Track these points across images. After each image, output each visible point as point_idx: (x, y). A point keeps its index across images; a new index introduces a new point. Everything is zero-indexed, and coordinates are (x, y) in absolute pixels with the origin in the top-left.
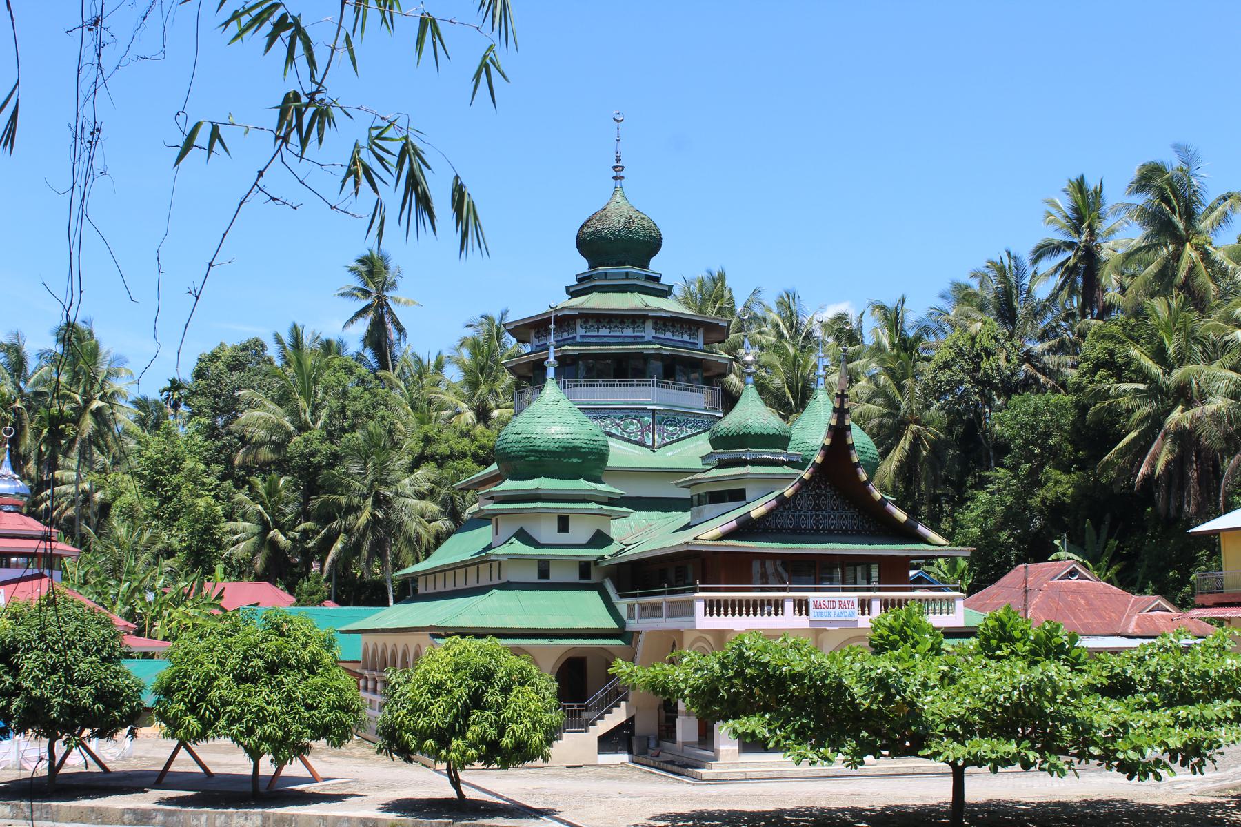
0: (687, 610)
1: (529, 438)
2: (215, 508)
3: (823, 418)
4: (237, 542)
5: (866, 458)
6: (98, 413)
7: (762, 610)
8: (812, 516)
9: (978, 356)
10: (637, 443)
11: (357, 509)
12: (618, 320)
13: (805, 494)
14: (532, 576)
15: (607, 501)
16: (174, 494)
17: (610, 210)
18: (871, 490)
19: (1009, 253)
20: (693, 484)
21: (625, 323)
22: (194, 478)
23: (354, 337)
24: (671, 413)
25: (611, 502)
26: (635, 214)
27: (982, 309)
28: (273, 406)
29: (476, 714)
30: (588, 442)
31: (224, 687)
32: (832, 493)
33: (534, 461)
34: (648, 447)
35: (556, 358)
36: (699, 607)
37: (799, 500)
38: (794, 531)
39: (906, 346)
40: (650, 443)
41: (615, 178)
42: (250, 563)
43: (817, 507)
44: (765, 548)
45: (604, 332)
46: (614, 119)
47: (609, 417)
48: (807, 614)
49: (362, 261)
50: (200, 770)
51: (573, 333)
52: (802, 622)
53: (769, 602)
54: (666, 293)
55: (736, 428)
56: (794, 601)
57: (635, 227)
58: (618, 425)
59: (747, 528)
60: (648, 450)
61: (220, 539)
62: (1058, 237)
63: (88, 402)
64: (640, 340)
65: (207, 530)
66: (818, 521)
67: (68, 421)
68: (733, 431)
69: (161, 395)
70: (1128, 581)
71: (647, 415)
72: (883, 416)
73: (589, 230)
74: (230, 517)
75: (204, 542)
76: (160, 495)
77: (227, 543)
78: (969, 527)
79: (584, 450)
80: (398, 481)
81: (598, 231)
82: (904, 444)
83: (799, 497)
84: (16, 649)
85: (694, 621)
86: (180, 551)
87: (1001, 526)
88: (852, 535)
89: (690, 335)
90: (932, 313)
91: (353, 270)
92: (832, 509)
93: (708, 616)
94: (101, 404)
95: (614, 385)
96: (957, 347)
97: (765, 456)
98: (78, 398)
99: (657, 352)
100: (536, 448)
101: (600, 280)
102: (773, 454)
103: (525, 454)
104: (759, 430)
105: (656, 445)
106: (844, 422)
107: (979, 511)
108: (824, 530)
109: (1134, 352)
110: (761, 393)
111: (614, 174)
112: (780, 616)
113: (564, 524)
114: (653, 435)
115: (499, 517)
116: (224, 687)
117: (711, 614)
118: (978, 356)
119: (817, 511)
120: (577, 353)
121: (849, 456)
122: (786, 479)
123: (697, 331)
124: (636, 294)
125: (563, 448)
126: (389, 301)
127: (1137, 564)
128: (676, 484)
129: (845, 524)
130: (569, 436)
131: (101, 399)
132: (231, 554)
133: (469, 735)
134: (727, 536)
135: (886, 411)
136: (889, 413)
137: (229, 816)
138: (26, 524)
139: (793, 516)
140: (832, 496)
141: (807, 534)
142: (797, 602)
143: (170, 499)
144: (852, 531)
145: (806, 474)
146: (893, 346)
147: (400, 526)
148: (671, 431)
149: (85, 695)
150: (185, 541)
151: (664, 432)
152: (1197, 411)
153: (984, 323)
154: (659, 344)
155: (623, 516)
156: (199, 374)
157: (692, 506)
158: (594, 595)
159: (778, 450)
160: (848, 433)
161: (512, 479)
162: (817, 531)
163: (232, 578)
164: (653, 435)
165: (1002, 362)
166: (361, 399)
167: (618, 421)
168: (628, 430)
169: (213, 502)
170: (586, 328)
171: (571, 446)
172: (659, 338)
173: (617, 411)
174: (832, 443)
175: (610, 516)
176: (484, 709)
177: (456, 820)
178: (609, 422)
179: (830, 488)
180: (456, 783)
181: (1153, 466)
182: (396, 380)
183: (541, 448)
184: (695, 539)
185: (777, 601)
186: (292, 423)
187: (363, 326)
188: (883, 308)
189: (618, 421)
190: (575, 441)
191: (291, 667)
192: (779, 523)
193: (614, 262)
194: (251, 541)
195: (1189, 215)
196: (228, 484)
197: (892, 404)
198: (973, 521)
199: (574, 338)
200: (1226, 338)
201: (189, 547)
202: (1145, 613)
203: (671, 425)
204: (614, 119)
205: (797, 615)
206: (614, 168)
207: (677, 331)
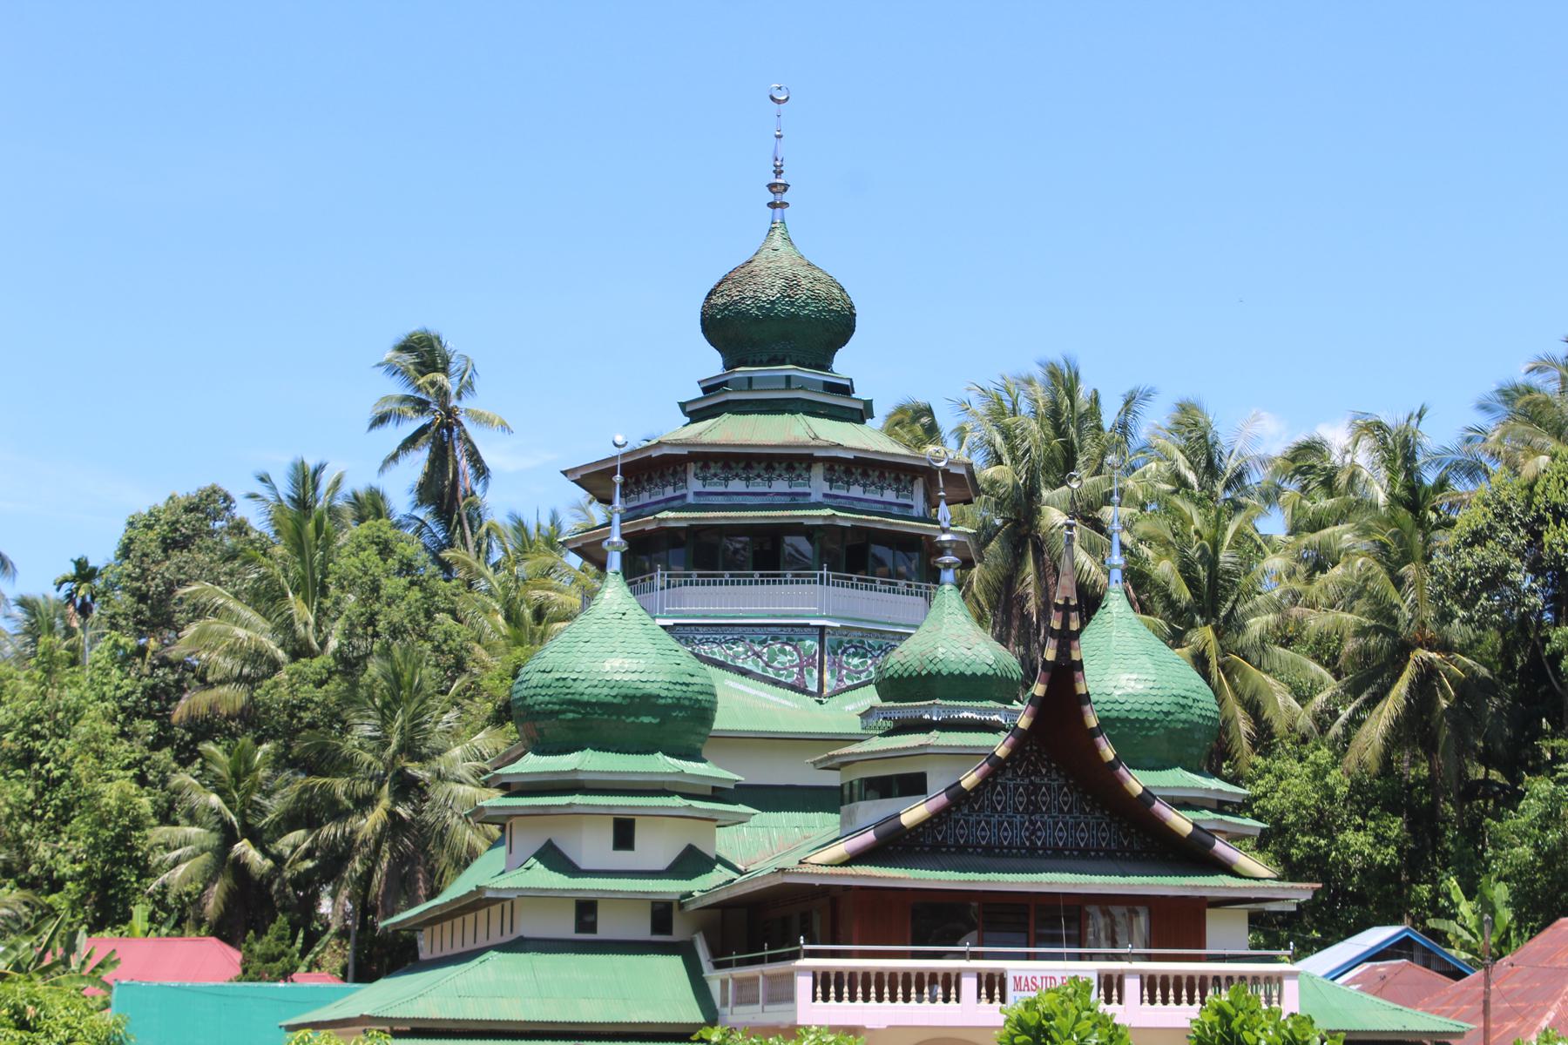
0: (783, 992)
1: (564, 679)
2: (136, 800)
3: (1114, 644)
4: (177, 862)
5: (1191, 717)
7: (920, 991)
8: (1022, 824)
9: (1541, 520)
10: (792, 687)
11: (365, 803)
12: (763, 465)
13: (1011, 784)
14: (565, 927)
15: (709, 793)
17: (760, 264)
18: (1122, 777)
20: (842, 765)
21: (774, 469)
24: (855, 633)
25: (718, 794)
28: (248, 613)
30: (671, 687)
32: (1061, 781)
33: (573, 720)
34: (811, 694)
35: (623, 536)
36: (804, 985)
37: (999, 794)
38: (989, 851)
39: (1413, 499)
40: (814, 688)
41: (773, 205)
42: (198, 902)
43: (1033, 808)
44: (875, 877)
45: (737, 485)
46: (772, 98)
47: (741, 639)
48: (1003, 1000)
49: (405, 347)
51: (682, 488)
52: (990, 1015)
54: (861, 414)
55: (917, 664)
56: (979, 976)
57: (802, 295)
60: (811, 701)
61: (146, 856)
64: (801, 500)
65: (122, 840)
66: (1033, 833)
68: (911, 669)
69: (58, 589)
71: (810, 636)
73: (720, 301)
74: (166, 816)
75: (117, 862)
77: (159, 865)
78: (1512, 846)
79: (663, 701)
80: (440, 752)
81: (736, 303)
82: (1401, 688)
83: (999, 788)
85: (794, 1011)
86: (72, 879)
89: (897, 490)
90: (1469, 440)
91: (392, 369)
92: (1061, 810)
93: (819, 1002)
95: (751, 583)
96: (1500, 503)
97: (965, 714)
99: (828, 522)
100: (577, 697)
101: (736, 390)
102: (978, 710)
103: (557, 707)
104: (957, 668)
105: (826, 691)
106: (1070, 655)
107: (1531, 815)
108: (1045, 850)
111: (771, 198)
112: (953, 1003)
113: (624, 835)
114: (821, 672)
115: (514, 820)
117: (826, 998)
119: (1033, 813)
120: (684, 524)
121: (1080, 717)
122: (965, 756)
123: (912, 482)
124: (800, 416)
125: (625, 697)
126: (462, 418)
128: (814, 763)
129: (1083, 838)
130: (635, 677)
132: (164, 886)
134: (857, 858)
136: (1374, 626)
139: (988, 823)
140: (1060, 788)
141: (1014, 856)
142: (984, 979)
144: (1097, 851)
145: (1000, 744)
146: (1394, 499)
147: (441, 835)
148: (855, 666)
150: (81, 861)
151: (841, 667)
153: (1554, 456)
154: (832, 507)
155: (740, 820)
156: (126, 551)
157: (843, 804)
158: (676, 963)
159: (991, 704)
160: (1078, 674)
161: (537, 753)
162: (1032, 851)
163: (164, 930)
164: (821, 672)
166: (403, 599)
167: (757, 648)
168: (775, 664)
169: (133, 788)
170: (704, 479)
171: (639, 693)
172: (837, 497)
173: (757, 629)
174: (1048, 692)
175: (715, 820)
178: (741, 649)
179: (1058, 773)
183: (585, 698)
184: (801, 862)
185: (947, 976)
186: (282, 645)
187: (417, 463)
189: (757, 648)
190: (648, 686)
192: (1061, 839)
193: (765, 359)
196: (165, 756)
197: (1384, 614)
198: (1523, 835)
199: (684, 496)
201: (88, 871)
203: (855, 655)
204: (772, 98)
205: (1146, 1004)
206: (771, 186)
207: (873, 483)
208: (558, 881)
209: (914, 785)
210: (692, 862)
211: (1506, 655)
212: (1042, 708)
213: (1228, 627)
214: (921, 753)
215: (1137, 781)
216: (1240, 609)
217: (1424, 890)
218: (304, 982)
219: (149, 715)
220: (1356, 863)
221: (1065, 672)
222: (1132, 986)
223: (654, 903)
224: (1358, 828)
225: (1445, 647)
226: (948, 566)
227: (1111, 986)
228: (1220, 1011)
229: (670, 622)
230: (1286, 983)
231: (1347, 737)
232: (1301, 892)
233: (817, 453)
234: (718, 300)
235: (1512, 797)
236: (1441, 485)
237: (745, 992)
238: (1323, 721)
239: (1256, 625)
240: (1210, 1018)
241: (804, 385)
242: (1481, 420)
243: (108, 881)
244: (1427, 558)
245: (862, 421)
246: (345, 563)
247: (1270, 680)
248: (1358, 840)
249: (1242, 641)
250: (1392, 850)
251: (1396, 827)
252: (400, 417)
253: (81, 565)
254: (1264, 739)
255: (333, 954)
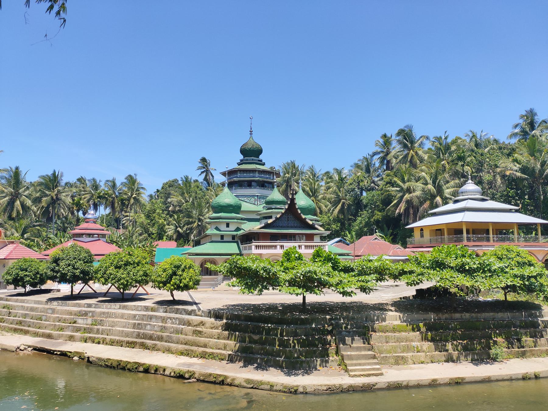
0: (250, 248)
6: (135, 198)
7: (271, 248)
10: (253, 204)
11: (195, 222)
16: (154, 219)
19: (369, 154)
22: (159, 215)
23: (201, 179)
26: (255, 143)
27: (362, 170)
29: (174, 277)
31: (112, 270)
36: (253, 247)
38: (281, 227)
39: (342, 179)
41: (250, 134)
42: (172, 236)
43: (288, 220)
45: (245, 175)
48: (284, 249)
50: (94, 292)
53: (273, 246)
54: (264, 164)
57: (255, 147)
58: (248, 199)
59: (267, 226)
62: (379, 150)
63: (132, 195)
65: (162, 228)
67: (126, 200)
70: (394, 241)
72: (335, 198)
74: (168, 225)
75: (161, 231)
76: (150, 219)
80: (205, 215)
82: (340, 205)
84: (59, 260)
87: (365, 226)
88: (298, 228)
91: (200, 162)
94: (135, 196)
97: (278, 207)
98: (129, 194)
101: (245, 161)
102: (280, 206)
107: (358, 222)
109: (396, 179)
110: (304, 192)
113: (228, 225)
116: (112, 270)
118: (360, 182)
122: (278, 213)
127: (397, 236)
129: (296, 225)
131: (136, 194)
133: (171, 283)
134: (261, 228)
135: (336, 196)
137: (111, 305)
138: (96, 226)
143: (153, 220)
145: (283, 211)
149: (77, 272)
152: (411, 195)
153: (361, 173)
155: (245, 223)
156: (163, 188)
158: (236, 244)
159: (282, 205)
162: (288, 227)
165: (366, 183)
169: (163, 221)
176: (176, 275)
177: (168, 306)
180: (172, 296)
181: (400, 210)
182: (212, 190)
185: (275, 246)
187: (204, 175)
188: (337, 169)
191: (131, 264)
194: (173, 231)
195: (412, 142)
196: (168, 216)
200: (420, 175)
201: (157, 232)
202: (395, 250)
206: (250, 131)
208: (218, 232)
209: (270, 217)
210: (238, 229)
211: (354, 201)
212: (289, 205)
213: (316, 197)
214: (271, 213)
215: (303, 217)
216: (318, 195)
217: (343, 233)
218: (186, 247)
219: (166, 210)
220: (333, 229)
221: (293, 200)
222: (303, 247)
223: (232, 235)
224: (334, 225)
225: (346, 200)
226: (275, 185)
227: (300, 247)
228: (317, 251)
229: (235, 195)
230: (302, 246)
231: (332, 212)
232: (328, 233)
233: (257, 170)
234: (242, 148)
235: (355, 220)
236: (345, 177)
237: (245, 249)
238: (329, 210)
239: (320, 197)
240: (316, 252)
241: (255, 160)
242: (351, 168)
243: (160, 234)
244: (344, 187)
245: (264, 165)
246: (192, 189)
247: (322, 204)
248: (334, 226)
249: (318, 199)
250: (339, 228)
251: (339, 225)
252: (202, 169)
253: (158, 190)
254: (321, 212)
255: (191, 243)
